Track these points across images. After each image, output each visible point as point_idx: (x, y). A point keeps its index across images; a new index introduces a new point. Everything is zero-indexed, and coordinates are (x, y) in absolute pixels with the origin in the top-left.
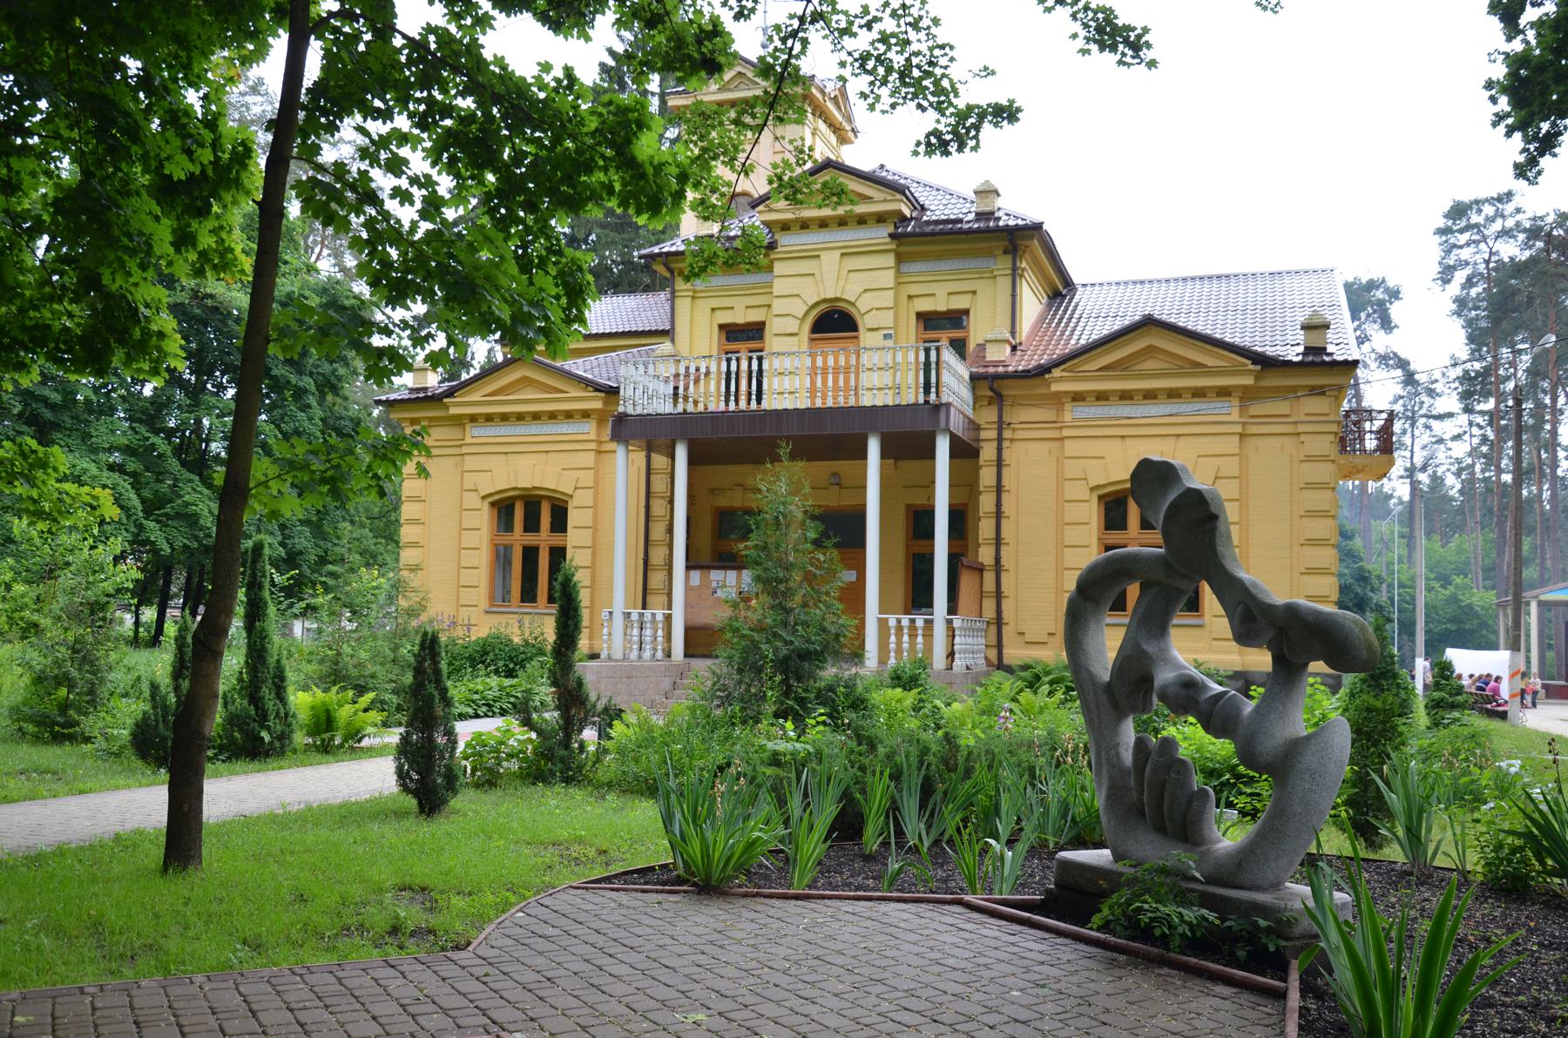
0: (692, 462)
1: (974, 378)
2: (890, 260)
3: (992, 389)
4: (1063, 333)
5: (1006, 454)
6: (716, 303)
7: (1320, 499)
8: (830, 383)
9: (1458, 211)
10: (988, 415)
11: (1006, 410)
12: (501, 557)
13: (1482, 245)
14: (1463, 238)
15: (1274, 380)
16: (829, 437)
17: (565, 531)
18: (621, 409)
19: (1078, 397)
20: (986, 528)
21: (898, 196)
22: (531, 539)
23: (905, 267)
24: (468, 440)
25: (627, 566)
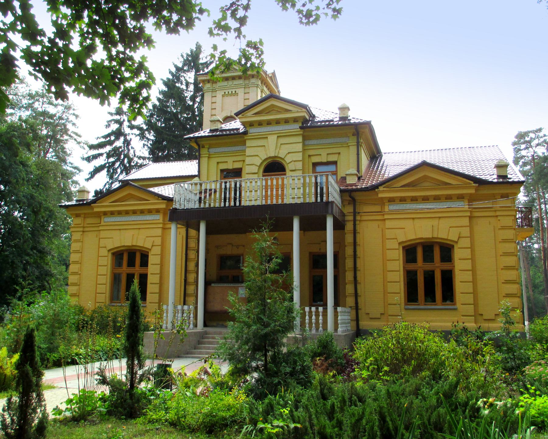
0: (208, 233)
1: (341, 191)
2: (300, 139)
3: (350, 197)
4: (380, 172)
5: (358, 227)
6: (219, 160)
7: (510, 247)
8: (269, 193)
9: (521, 136)
10: (349, 209)
11: (357, 206)
12: (116, 279)
13: (530, 149)
14: (523, 146)
15: (485, 191)
16: (276, 217)
17: (147, 266)
18: (174, 206)
19: (391, 200)
20: (349, 263)
21: (304, 110)
22: (131, 270)
23: (307, 142)
24: (102, 223)
25: (176, 283)
